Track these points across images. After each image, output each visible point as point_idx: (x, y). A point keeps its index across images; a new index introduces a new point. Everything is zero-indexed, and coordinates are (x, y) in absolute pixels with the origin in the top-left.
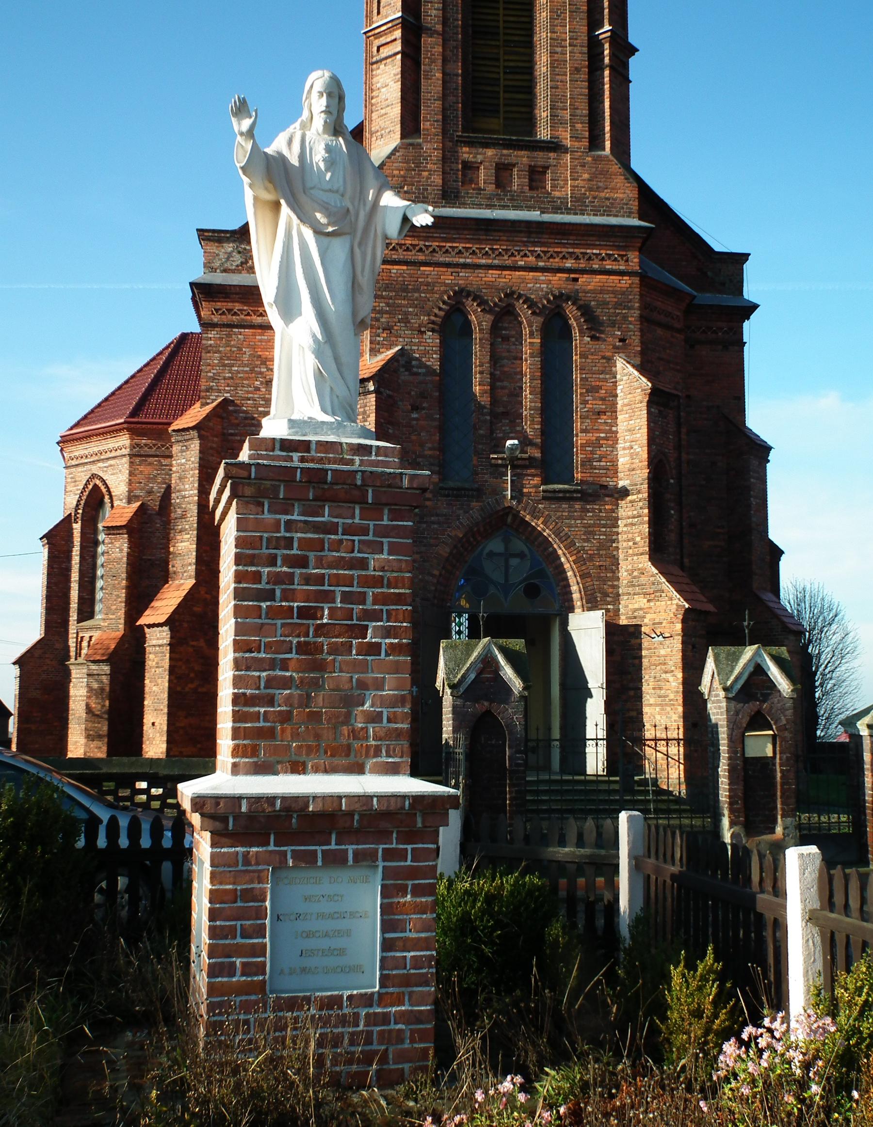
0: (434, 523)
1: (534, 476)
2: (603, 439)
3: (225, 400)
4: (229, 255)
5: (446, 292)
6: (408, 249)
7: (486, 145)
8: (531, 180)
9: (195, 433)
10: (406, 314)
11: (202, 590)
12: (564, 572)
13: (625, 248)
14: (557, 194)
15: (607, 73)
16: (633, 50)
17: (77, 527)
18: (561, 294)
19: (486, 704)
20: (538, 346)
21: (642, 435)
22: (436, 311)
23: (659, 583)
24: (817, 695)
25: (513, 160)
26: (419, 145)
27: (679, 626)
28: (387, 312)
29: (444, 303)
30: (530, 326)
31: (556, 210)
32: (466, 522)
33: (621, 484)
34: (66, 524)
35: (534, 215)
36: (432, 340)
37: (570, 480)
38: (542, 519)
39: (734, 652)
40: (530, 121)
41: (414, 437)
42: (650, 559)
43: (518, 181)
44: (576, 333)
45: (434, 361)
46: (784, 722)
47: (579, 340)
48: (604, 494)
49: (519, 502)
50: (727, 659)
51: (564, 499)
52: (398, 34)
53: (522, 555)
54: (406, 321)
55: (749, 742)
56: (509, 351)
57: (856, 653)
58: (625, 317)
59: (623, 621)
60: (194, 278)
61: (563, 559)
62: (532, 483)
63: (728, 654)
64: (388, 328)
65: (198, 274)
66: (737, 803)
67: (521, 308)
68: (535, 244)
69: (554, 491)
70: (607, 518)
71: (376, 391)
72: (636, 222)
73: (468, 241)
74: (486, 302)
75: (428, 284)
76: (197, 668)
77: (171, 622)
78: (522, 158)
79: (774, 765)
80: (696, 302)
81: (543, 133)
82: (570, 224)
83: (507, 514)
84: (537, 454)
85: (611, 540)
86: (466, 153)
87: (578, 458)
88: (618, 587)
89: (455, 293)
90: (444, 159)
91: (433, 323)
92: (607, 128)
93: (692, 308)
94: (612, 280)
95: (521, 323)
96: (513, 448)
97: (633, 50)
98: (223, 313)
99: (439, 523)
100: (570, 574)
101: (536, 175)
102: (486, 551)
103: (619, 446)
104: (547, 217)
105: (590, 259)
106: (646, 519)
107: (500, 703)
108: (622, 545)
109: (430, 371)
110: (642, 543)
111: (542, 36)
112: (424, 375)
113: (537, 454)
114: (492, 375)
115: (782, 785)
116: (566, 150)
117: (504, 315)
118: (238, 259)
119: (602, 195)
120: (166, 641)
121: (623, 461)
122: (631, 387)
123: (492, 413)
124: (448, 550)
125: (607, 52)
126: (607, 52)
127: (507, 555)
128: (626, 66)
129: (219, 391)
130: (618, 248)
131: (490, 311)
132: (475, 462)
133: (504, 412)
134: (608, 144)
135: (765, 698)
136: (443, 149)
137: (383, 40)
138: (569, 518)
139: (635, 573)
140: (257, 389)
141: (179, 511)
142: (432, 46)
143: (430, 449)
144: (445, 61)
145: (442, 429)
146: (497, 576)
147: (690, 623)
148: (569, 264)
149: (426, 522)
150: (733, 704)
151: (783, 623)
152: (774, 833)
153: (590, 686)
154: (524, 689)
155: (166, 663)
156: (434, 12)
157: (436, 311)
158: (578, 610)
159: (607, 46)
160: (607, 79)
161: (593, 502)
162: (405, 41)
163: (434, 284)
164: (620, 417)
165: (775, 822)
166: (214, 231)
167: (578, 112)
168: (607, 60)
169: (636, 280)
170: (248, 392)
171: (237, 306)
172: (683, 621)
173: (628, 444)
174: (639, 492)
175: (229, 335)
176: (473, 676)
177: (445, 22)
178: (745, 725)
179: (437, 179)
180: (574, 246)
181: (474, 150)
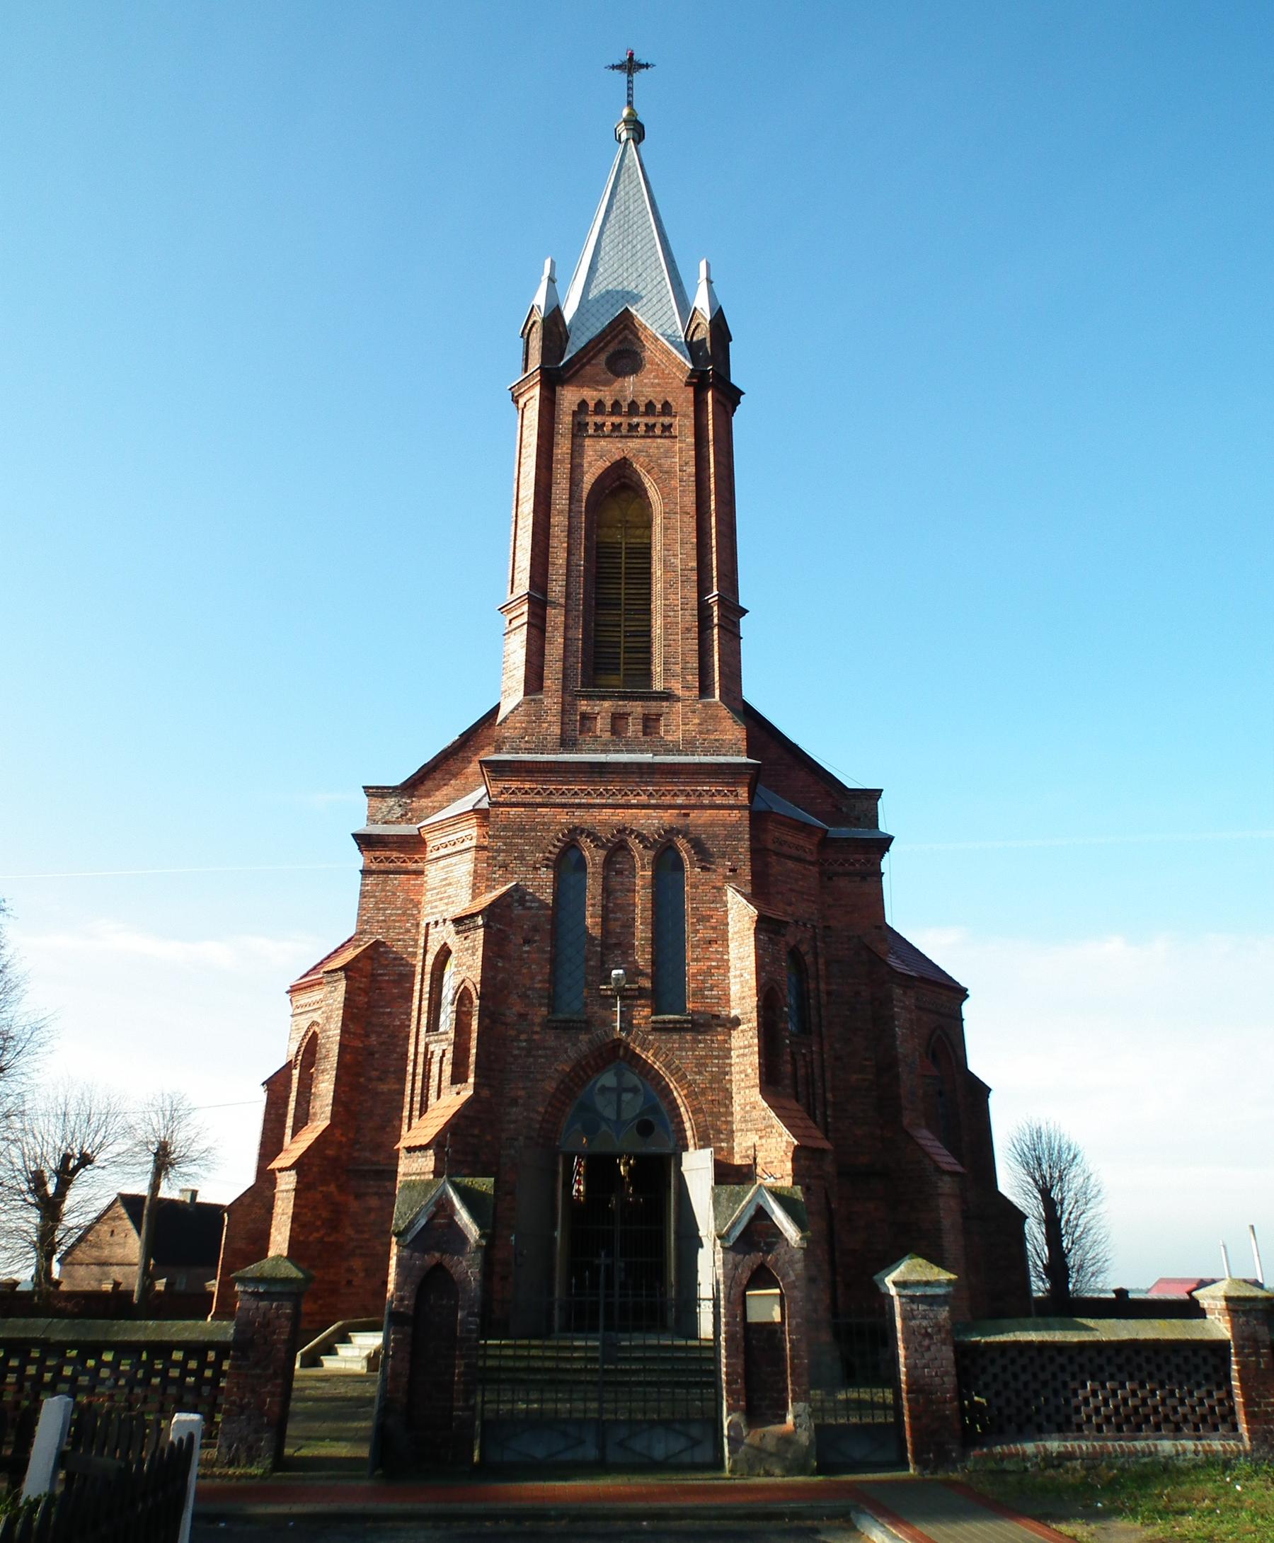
0: (541, 1056)
1: (644, 1006)
2: (715, 967)
3: (377, 942)
4: (391, 808)
5: (561, 830)
6: (526, 793)
7: (603, 698)
8: (645, 727)
9: (342, 974)
10: (522, 851)
11: (338, 1133)
12: (678, 1107)
13: (734, 784)
14: (670, 738)
15: (716, 631)
16: (744, 612)
17: (296, 1073)
18: (672, 829)
19: (437, 1255)
20: (649, 880)
21: (751, 963)
22: (551, 848)
23: (770, 1118)
24: (1064, 1245)
25: (628, 710)
26: (540, 700)
27: (789, 1165)
28: (503, 851)
29: (559, 840)
30: (642, 860)
31: (669, 752)
32: (572, 1054)
33: (734, 1013)
34: (289, 1067)
35: (647, 757)
36: (546, 875)
37: (682, 1010)
38: (651, 1051)
39: (738, 1192)
40: (648, 675)
41: (525, 971)
42: (761, 1092)
43: (633, 728)
44: (687, 866)
45: (547, 896)
46: (793, 1278)
47: (692, 872)
48: (717, 1023)
49: (628, 1034)
50: (728, 1200)
51: (675, 1030)
52: (525, 608)
53: (634, 1090)
54: (521, 858)
55: (751, 1303)
56: (622, 884)
57: (1100, 1198)
58: (735, 849)
59: (738, 1161)
60: (357, 830)
61: (675, 1094)
62: (642, 1015)
63: (731, 1195)
64: (504, 866)
65: (362, 827)
66: (736, 1382)
67: (634, 843)
68: (647, 783)
69: (664, 1022)
70: (719, 1049)
71: (485, 926)
72: (744, 759)
73: (584, 783)
74: (599, 838)
75: (544, 824)
76: (325, 1214)
77: (298, 1166)
78: (637, 708)
79: (783, 1333)
80: (829, 835)
81: (658, 686)
82: (679, 764)
83: (619, 1046)
84: (647, 984)
85: (724, 1072)
86: (584, 706)
87: (691, 986)
88: (731, 1123)
89: (569, 831)
90: (563, 711)
91: (548, 859)
92: (717, 678)
93: (826, 842)
94: (724, 814)
95: (633, 857)
96: (618, 979)
97: (744, 612)
98: (381, 861)
99: (545, 1056)
100: (682, 1109)
101: (650, 723)
102: (599, 1085)
103: (731, 974)
104: (658, 759)
105: (700, 795)
106: (756, 1049)
107: (453, 1255)
108: (735, 1077)
109: (543, 905)
110: (752, 1075)
111: (657, 604)
112: (538, 908)
113: (647, 984)
114: (604, 907)
115: (792, 1358)
116: (678, 699)
117: (617, 848)
118: (398, 811)
119: (712, 737)
120: (293, 1186)
121: (735, 989)
122: (740, 915)
123: (604, 945)
124: (554, 1085)
125: (715, 614)
126: (715, 614)
127: (620, 1090)
128: (737, 625)
129: (372, 933)
130: (728, 784)
131: (603, 847)
132: (585, 994)
133: (615, 943)
134: (717, 692)
135: (770, 1248)
136: (563, 704)
137: (514, 614)
138: (681, 1049)
139: (748, 1108)
140: (408, 931)
141: (324, 1051)
142: (555, 617)
143: (540, 981)
144: (566, 628)
145: (554, 961)
146: (610, 1113)
147: (802, 1162)
148: (680, 801)
149: (533, 1056)
150: (731, 1255)
151: (935, 1162)
152: (785, 1422)
153: (701, 1233)
154: (481, 1236)
155: (290, 1212)
156: (558, 588)
157: (551, 848)
158: (691, 1149)
159: (715, 608)
160: (716, 637)
161: (705, 1032)
162: (531, 613)
163: (549, 824)
164: (731, 945)
165: (785, 1408)
166: (377, 788)
167: (689, 665)
168: (716, 621)
169: (746, 813)
170: (399, 934)
171: (395, 855)
172: (794, 1160)
173: (738, 973)
174: (749, 1021)
175: (385, 882)
176: (423, 1222)
177: (568, 596)
178: (745, 1282)
179: (556, 730)
180: (684, 783)
181: (591, 703)
